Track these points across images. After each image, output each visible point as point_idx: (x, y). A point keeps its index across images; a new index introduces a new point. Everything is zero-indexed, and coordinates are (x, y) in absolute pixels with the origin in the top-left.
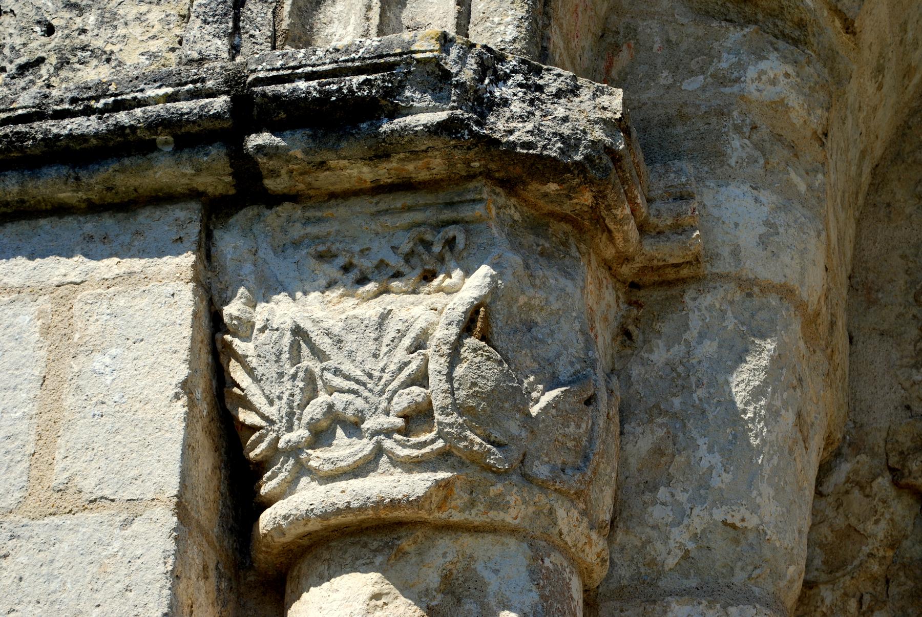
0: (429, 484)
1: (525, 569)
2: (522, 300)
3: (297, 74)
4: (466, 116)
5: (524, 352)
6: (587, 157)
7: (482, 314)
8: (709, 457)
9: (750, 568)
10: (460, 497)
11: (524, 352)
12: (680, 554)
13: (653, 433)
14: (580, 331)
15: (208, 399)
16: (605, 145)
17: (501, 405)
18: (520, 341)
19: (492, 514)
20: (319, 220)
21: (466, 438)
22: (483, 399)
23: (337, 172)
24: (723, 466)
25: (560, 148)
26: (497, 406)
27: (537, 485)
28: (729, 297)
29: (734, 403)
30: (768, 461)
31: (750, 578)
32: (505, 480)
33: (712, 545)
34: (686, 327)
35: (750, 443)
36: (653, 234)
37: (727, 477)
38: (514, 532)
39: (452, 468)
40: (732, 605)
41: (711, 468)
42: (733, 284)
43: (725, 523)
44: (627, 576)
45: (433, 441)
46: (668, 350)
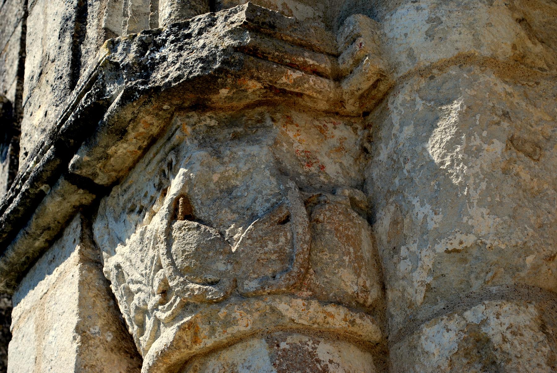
0: (174, 331)
1: (268, 357)
2: (216, 177)
4: (134, 83)
5: (223, 211)
6: (223, 62)
8: (423, 210)
9: (482, 275)
10: (204, 330)
11: (223, 211)
12: (424, 289)
13: (389, 210)
15: (114, 328)
16: (234, 47)
17: (206, 256)
18: (220, 205)
19: (229, 330)
20: (129, 187)
21: (188, 289)
22: (192, 258)
24: (433, 211)
25: (201, 68)
26: (203, 258)
27: (253, 297)
28: (416, 87)
29: (433, 161)
30: (475, 189)
31: (486, 282)
33: (443, 272)
34: (392, 125)
35: (453, 184)
37: (439, 218)
38: (253, 335)
39: (192, 312)
40: (466, 310)
41: (425, 217)
42: (416, 78)
43: (447, 251)
44: (401, 321)
45: (175, 301)
46: (387, 148)
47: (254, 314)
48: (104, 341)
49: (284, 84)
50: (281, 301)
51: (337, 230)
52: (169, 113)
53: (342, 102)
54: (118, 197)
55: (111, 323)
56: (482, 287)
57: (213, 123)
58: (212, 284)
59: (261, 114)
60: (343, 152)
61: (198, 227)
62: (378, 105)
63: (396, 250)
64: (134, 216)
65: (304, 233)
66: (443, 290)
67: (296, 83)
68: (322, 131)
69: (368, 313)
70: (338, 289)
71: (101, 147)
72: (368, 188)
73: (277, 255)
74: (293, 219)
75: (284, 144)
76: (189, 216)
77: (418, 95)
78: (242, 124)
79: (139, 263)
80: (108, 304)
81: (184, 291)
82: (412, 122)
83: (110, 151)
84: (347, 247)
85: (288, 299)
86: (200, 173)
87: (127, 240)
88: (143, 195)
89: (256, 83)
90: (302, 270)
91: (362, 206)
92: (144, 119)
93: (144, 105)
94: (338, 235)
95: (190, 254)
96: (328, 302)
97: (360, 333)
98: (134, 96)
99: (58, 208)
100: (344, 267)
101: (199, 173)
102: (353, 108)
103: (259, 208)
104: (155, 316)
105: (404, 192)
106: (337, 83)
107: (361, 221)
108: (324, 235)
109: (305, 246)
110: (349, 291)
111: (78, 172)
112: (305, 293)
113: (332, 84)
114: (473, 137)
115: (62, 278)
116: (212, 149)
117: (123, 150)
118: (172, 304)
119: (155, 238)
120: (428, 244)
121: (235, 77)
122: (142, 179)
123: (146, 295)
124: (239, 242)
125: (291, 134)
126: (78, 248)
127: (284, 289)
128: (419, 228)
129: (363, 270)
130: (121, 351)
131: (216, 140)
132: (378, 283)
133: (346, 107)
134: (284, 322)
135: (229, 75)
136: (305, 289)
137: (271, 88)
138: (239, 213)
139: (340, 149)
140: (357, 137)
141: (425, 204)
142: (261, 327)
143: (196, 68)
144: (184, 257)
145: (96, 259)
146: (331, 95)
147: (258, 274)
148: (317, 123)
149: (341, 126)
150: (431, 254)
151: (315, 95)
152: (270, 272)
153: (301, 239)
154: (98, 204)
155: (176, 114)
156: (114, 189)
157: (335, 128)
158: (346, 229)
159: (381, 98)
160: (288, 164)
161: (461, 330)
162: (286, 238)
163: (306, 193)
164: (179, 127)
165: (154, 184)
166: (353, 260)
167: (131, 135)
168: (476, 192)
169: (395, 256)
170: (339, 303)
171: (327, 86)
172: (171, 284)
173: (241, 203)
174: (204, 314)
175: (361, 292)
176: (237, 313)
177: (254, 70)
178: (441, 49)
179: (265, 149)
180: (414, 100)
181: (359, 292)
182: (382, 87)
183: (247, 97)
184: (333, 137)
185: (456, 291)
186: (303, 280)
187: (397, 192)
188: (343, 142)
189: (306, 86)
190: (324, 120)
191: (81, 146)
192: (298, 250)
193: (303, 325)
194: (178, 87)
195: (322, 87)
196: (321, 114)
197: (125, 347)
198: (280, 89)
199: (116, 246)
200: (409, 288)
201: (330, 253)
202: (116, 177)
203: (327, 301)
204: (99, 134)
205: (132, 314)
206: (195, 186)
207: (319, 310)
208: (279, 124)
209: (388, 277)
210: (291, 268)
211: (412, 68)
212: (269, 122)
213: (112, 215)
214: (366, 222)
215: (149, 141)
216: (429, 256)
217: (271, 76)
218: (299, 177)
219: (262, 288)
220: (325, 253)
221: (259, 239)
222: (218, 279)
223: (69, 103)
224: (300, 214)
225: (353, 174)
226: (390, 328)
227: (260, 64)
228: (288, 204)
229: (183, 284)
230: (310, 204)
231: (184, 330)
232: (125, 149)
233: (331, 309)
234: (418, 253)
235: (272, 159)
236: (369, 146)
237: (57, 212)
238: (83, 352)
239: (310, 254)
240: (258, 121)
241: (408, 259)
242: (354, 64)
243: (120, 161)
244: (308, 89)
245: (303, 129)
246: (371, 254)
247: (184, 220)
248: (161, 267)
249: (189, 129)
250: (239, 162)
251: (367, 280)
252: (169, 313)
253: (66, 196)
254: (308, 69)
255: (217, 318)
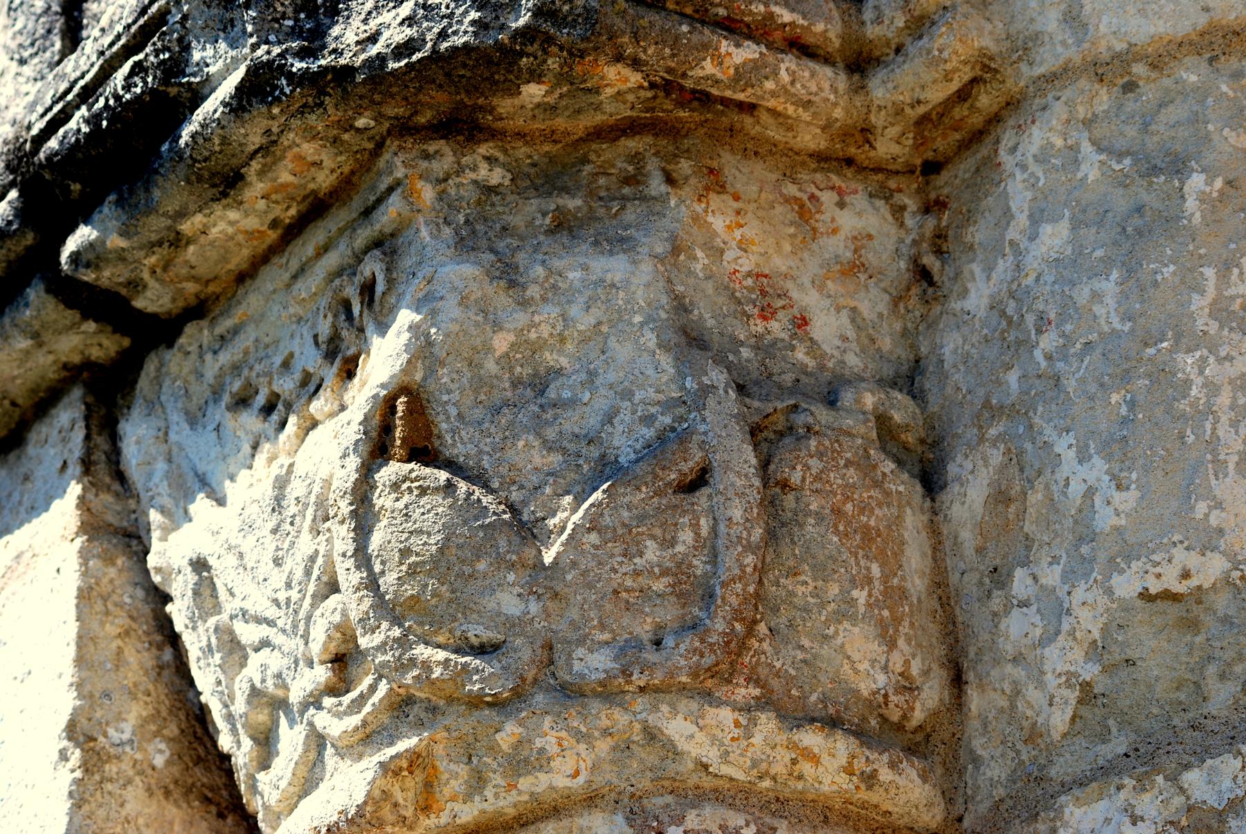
0: (370, 775)
2: (501, 342)
3: (69, 103)
4: (276, 50)
5: (521, 444)
7: (400, 408)
8: (1083, 471)
10: (454, 776)
11: (521, 444)
12: (1073, 696)
13: (985, 460)
14: (659, 346)
15: (172, 730)
17: (467, 570)
18: (511, 424)
19: (524, 783)
20: (236, 331)
21: (413, 662)
22: (429, 574)
23: (203, 239)
24: (1114, 477)
25: (473, 23)
26: (460, 575)
27: (597, 695)
28: (1081, 112)
32: (519, 710)
33: (1130, 654)
34: (1008, 214)
36: (892, 56)
37: (1127, 500)
38: (591, 800)
39: (420, 725)
40: (1187, 767)
41: (1090, 492)
42: (1083, 83)
43: (1145, 596)
44: (1003, 776)
45: (373, 688)
46: (989, 278)
47: (597, 743)
48: (145, 766)
49: (707, 78)
50: (675, 712)
51: (837, 512)
52: (370, 139)
53: (866, 133)
54: (201, 357)
55: (164, 713)
56: (1236, 702)
57: (497, 176)
58: (482, 650)
59: (636, 158)
60: (863, 277)
61: (449, 487)
62: (968, 147)
63: (999, 577)
64: (250, 421)
65: (747, 520)
66: (1128, 702)
67: (742, 76)
68: (804, 212)
69: (911, 750)
70: (833, 681)
71: (165, 214)
72: (927, 386)
73: (670, 580)
74: (719, 479)
75: (700, 254)
76: (422, 453)
77: (1086, 134)
78: (581, 187)
79: (267, 567)
80: (158, 658)
81: (403, 666)
82: (1067, 213)
83: (186, 227)
84: (862, 563)
85: (694, 705)
86: (457, 328)
87: (227, 483)
88: (278, 360)
89: (627, 72)
90: (738, 626)
91: (910, 438)
92: (296, 150)
93: (302, 113)
94: (841, 528)
95: (423, 562)
96: (804, 718)
97: (887, 806)
98: (276, 87)
99: (19, 367)
100: (854, 620)
101: (455, 328)
102: (895, 149)
103: (624, 442)
104: (311, 724)
105: (1031, 414)
106: (856, 77)
107: (904, 485)
108: (802, 526)
109: (750, 559)
110: (862, 686)
111: (88, 276)
112: (743, 691)
113: (842, 82)
114: (1236, 271)
115: (21, 568)
116: (492, 257)
117: (225, 229)
118: (363, 698)
119: (321, 503)
120: (1092, 570)
121: (571, 54)
122: (279, 320)
123: (286, 660)
124: (564, 536)
125: (718, 223)
126: (75, 489)
127: (684, 679)
128: (1069, 523)
129: (905, 628)
130: (192, 797)
131: (504, 229)
132: (942, 665)
133: (878, 145)
134: (681, 769)
135: (554, 49)
136: (742, 681)
137: (668, 87)
138: (564, 451)
139: (853, 269)
140: (902, 233)
141: (1090, 457)
142: (615, 781)
143: (460, 22)
144: (404, 568)
145: (125, 524)
146: (838, 113)
147: (613, 631)
148: (791, 190)
149: (859, 200)
150: (1099, 599)
151: (791, 110)
152: (647, 628)
153: (739, 538)
154: (138, 367)
155: (392, 145)
156: (190, 329)
157: (841, 205)
158: (862, 511)
159: (980, 127)
160: (706, 314)
161: (1172, 823)
162: (697, 534)
163: (756, 404)
164: (398, 183)
165: (316, 337)
166: (877, 600)
167: (255, 188)
168: (1237, 433)
169: (996, 593)
170: (833, 723)
171: (826, 86)
172: (364, 642)
173: (571, 422)
174: (455, 734)
175: (897, 692)
176: (549, 738)
177: (626, 39)
178: (1161, 7)
179: (647, 267)
180: (1074, 149)
181: (890, 692)
182: (985, 101)
183: (598, 108)
184: (835, 231)
185: (1162, 708)
186: (739, 655)
187: (1017, 412)
188: (863, 247)
189: (769, 85)
190: (810, 182)
191: (101, 203)
192: (729, 569)
193: (731, 779)
194: (405, 74)
195: (814, 89)
196: (803, 164)
197: (203, 785)
198: (694, 91)
199: (189, 497)
200: (1031, 687)
201: (815, 579)
202: (197, 296)
203: (801, 715)
204: (160, 180)
205: (239, 707)
206: (442, 364)
207: (778, 739)
208: (686, 191)
209: (972, 651)
210: (707, 621)
211: (1072, 54)
212: (656, 185)
213: (180, 405)
214: (919, 488)
215: (303, 207)
216: (1094, 606)
217: (673, 55)
218: (737, 353)
219: (623, 672)
220: (803, 578)
221: (620, 532)
222: (501, 637)
223: (73, 76)
224: (738, 463)
225: (886, 344)
226: (969, 792)
227: (644, 22)
228: (705, 433)
229: (401, 646)
230: (765, 433)
231: (396, 774)
232: (231, 223)
233: (811, 738)
234: (1062, 593)
235: (664, 300)
236: (938, 264)
237: (15, 378)
238: (87, 796)
239: (760, 582)
240: (628, 180)
241: (1034, 608)
242: (908, 27)
243: (213, 255)
244: (773, 94)
245: (752, 206)
246: (926, 581)
247: (409, 461)
248: (334, 588)
249: (428, 193)
250: (569, 302)
251: (914, 656)
252: (355, 720)
253: (47, 336)
254: (778, 35)
255: (493, 749)
